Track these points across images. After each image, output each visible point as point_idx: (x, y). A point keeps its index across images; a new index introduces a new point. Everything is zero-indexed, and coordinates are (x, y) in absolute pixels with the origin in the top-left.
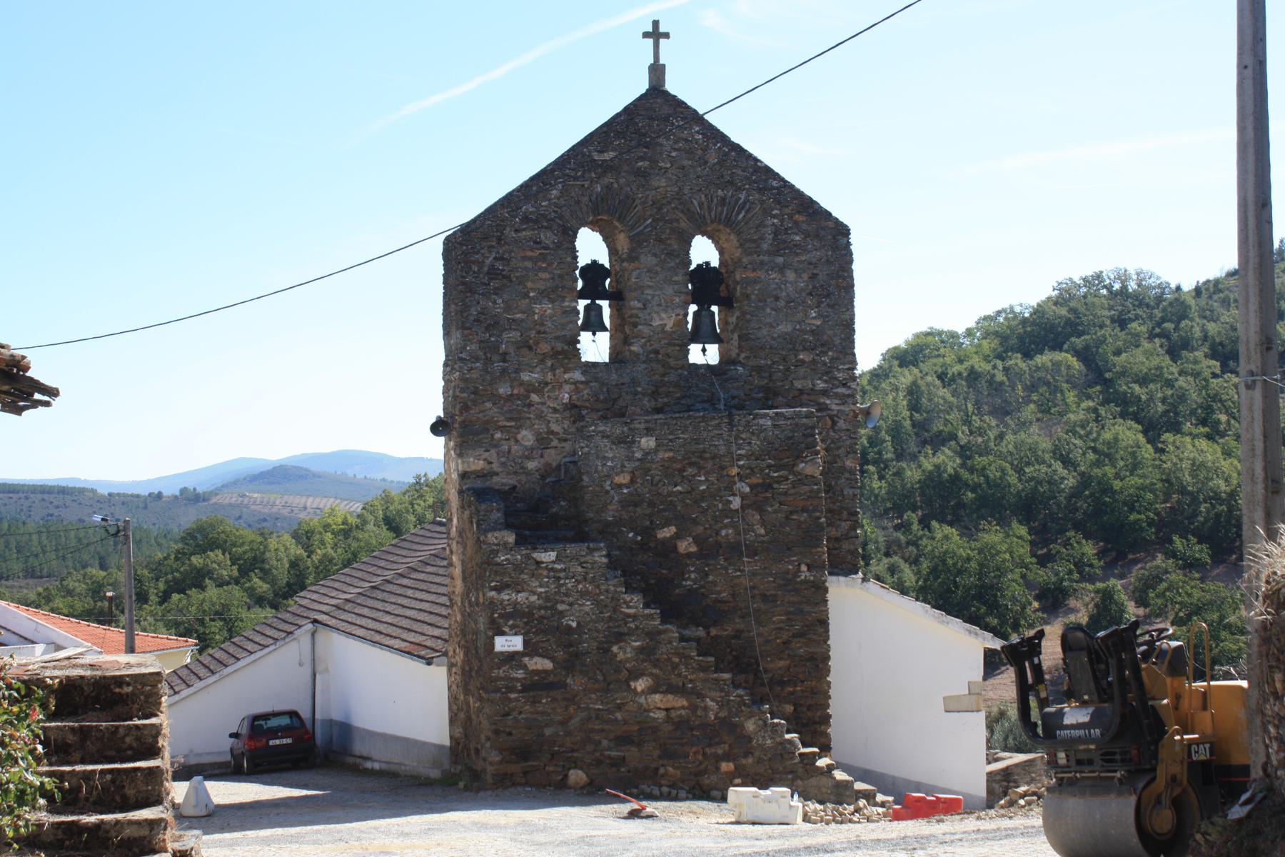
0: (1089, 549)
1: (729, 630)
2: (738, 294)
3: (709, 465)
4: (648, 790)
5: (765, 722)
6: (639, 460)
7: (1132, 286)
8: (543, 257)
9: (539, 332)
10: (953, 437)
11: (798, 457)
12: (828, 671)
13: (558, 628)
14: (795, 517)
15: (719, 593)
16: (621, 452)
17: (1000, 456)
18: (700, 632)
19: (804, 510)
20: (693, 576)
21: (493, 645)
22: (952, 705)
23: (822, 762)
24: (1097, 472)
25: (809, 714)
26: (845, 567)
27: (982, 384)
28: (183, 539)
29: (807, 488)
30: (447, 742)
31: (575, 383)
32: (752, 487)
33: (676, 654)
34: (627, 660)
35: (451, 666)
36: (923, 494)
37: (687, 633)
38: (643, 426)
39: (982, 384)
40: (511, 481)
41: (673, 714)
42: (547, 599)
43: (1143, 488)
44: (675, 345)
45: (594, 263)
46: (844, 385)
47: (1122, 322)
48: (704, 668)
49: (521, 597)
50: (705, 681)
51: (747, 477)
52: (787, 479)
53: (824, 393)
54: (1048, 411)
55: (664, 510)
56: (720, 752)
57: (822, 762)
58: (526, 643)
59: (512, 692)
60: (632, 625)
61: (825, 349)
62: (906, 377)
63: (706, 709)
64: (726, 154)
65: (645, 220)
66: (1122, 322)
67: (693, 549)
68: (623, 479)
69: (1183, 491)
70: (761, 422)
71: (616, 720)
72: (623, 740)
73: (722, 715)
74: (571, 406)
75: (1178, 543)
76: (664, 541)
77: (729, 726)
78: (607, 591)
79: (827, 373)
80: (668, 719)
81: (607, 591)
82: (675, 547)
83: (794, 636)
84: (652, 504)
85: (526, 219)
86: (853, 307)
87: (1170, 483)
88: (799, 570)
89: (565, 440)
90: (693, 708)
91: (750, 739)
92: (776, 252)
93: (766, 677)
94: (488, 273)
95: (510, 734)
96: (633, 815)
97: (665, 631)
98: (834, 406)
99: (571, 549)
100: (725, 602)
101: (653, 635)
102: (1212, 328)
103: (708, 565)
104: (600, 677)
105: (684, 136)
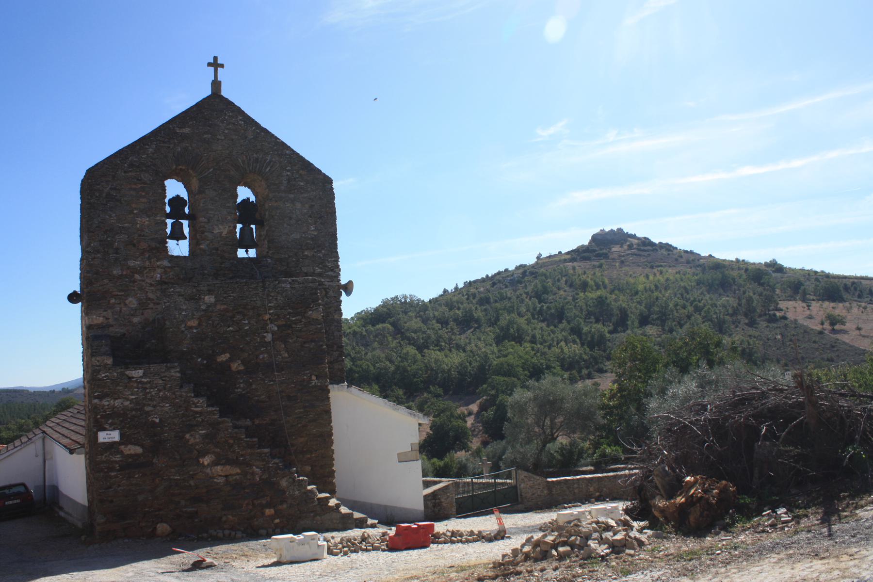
0: (401, 392)
2: (267, 216)
4: (214, 533)
5: (294, 479)
7: (408, 300)
9: (140, 235)
10: (350, 355)
17: (367, 360)
18: (248, 422)
20: (242, 386)
21: (96, 438)
22: (403, 458)
23: (333, 502)
24: (402, 364)
26: (338, 381)
27: (358, 336)
28: (56, 406)
30: (86, 503)
31: (164, 268)
32: (279, 327)
35: (86, 454)
37: (239, 423)
38: (206, 288)
39: (358, 336)
43: (418, 369)
45: (178, 196)
46: (332, 270)
47: (406, 313)
49: (117, 403)
53: (320, 275)
54: (382, 344)
56: (264, 502)
58: (121, 435)
60: (199, 419)
63: (253, 474)
65: (209, 169)
66: (406, 313)
67: (242, 368)
68: (193, 323)
69: (432, 370)
70: (283, 285)
71: (190, 486)
73: (265, 476)
74: (162, 282)
75: (432, 388)
78: (181, 396)
81: (181, 396)
82: (230, 367)
85: (131, 165)
87: (427, 367)
88: (310, 379)
89: (158, 304)
91: (284, 492)
95: (112, 501)
96: (198, 565)
99: (154, 368)
102: (436, 314)
104: (178, 457)
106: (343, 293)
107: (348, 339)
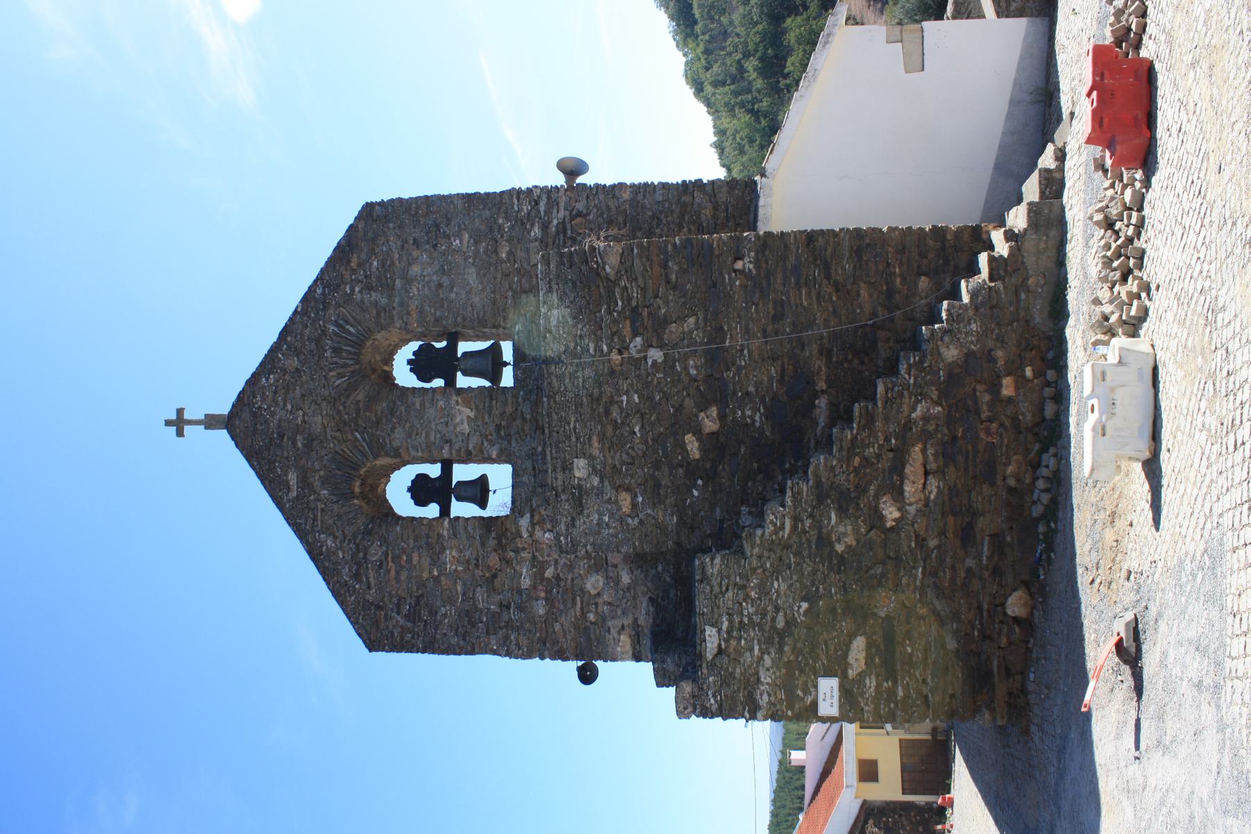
1: (819, 364)
3: (608, 389)
5: (944, 332)
6: (602, 481)
8: (396, 558)
9: (477, 566)
10: (739, 62)
11: (598, 274)
12: (876, 231)
13: (809, 628)
14: (673, 277)
15: (771, 378)
16: (592, 505)
19: (665, 266)
20: (748, 413)
22: (916, 62)
23: (1002, 248)
25: (931, 256)
29: (637, 262)
31: (533, 524)
32: (635, 334)
33: (849, 460)
34: (856, 531)
36: (770, 78)
38: (560, 475)
40: (644, 603)
41: (932, 466)
42: (769, 641)
44: (490, 406)
46: (537, 203)
48: (870, 419)
50: (887, 419)
51: (622, 340)
52: (626, 287)
53: (545, 227)
55: (665, 449)
56: (987, 398)
57: (1002, 248)
58: (828, 674)
59: (896, 695)
60: (808, 523)
61: (496, 227)
62: (709, 89)
63: (926, 418)
64: (289, 347)
67: (714, 411)
68: (625, 500)
70: (554, 322)
71: (938, 547)
72: (967, 535)
76: (704, 449)
77: (952, 385)
78: (760, 557)
79: (523, 224)
80: (941, 472)
81: (760, 557)
83: (828, 277)
84: (657, 465)
85: (357, 576)
86: (450, 196)
88: (742, 272)
90: (925, 436)
91: (970, 355)
92: (389, 288)
93: (882, 314)
94: (414, 622)
96: (1130, 653)
97: (817, 476)
98: (560, 214)
99: (702, 605)
100: (783, 370)
101: (821, 493)
103: (735, 393)
105: (271, 396)
106: (580, 180)
107: (716, 62)
